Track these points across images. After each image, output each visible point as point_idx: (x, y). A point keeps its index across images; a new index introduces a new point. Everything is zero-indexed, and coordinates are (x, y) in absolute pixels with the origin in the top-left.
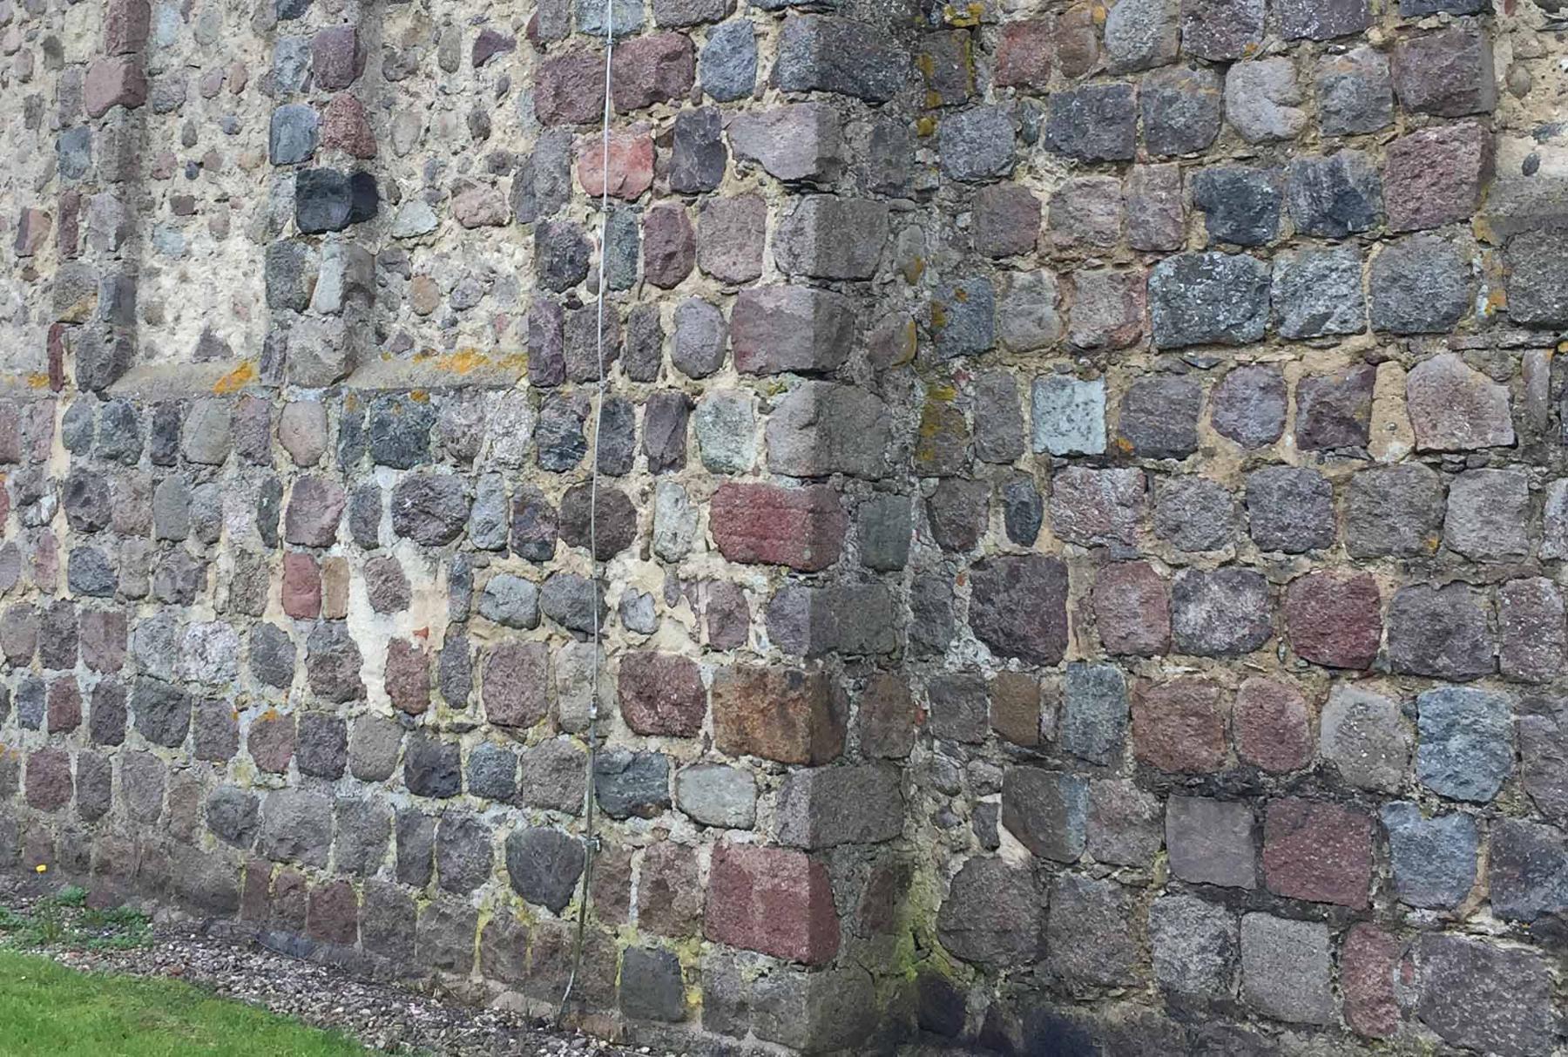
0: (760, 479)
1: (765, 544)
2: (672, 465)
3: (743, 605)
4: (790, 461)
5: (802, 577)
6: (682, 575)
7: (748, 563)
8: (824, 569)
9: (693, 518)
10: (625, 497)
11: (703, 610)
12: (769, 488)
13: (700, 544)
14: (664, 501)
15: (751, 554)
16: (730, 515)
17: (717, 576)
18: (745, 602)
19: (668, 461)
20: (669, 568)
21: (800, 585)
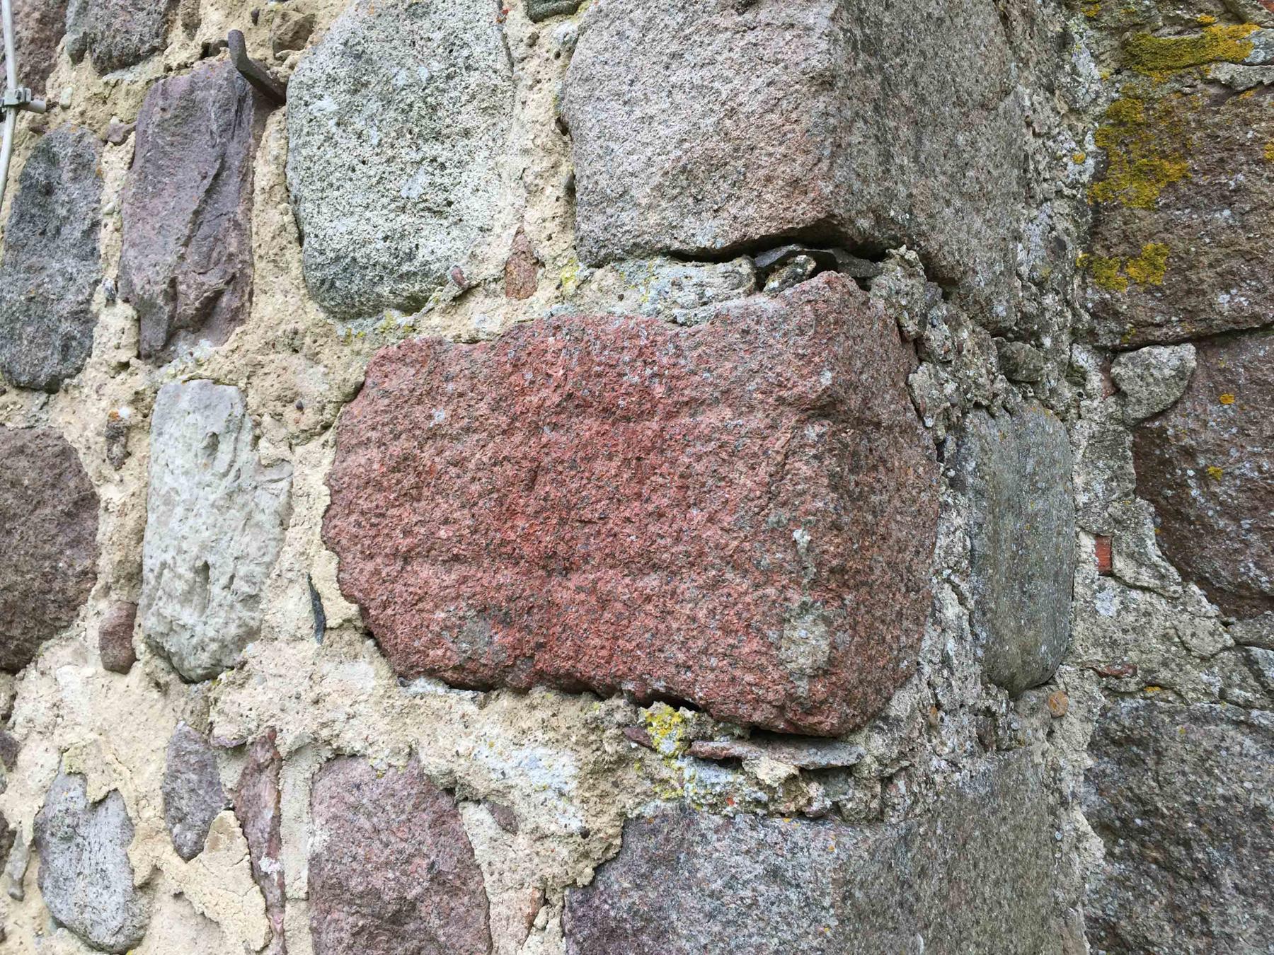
0: (541, 304)
1: (564, 591)
2: (206, 317)
3: (458, 879)
4: (688, 181)
5: (772, 767)
6: (225, 732)
7: (481, 683)
8: (877, 718)
9: (268, 502)
10: (67, 453)
11: (298, 885)
12: (579, 335)
13: (289, 608)
14: (171, 452)
15: (493, 643)
16: (410, 479)
17: (351, 739)
18: (468, 864)
19: (190, 303)
20: (185, 698)
21: (762, 810)
